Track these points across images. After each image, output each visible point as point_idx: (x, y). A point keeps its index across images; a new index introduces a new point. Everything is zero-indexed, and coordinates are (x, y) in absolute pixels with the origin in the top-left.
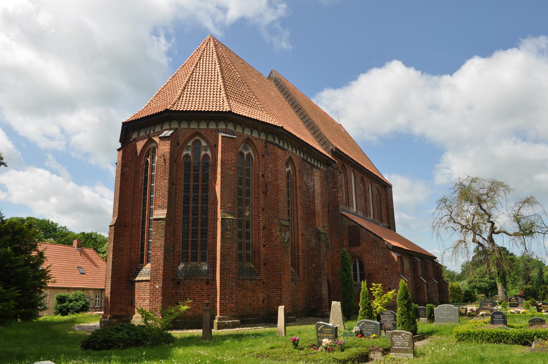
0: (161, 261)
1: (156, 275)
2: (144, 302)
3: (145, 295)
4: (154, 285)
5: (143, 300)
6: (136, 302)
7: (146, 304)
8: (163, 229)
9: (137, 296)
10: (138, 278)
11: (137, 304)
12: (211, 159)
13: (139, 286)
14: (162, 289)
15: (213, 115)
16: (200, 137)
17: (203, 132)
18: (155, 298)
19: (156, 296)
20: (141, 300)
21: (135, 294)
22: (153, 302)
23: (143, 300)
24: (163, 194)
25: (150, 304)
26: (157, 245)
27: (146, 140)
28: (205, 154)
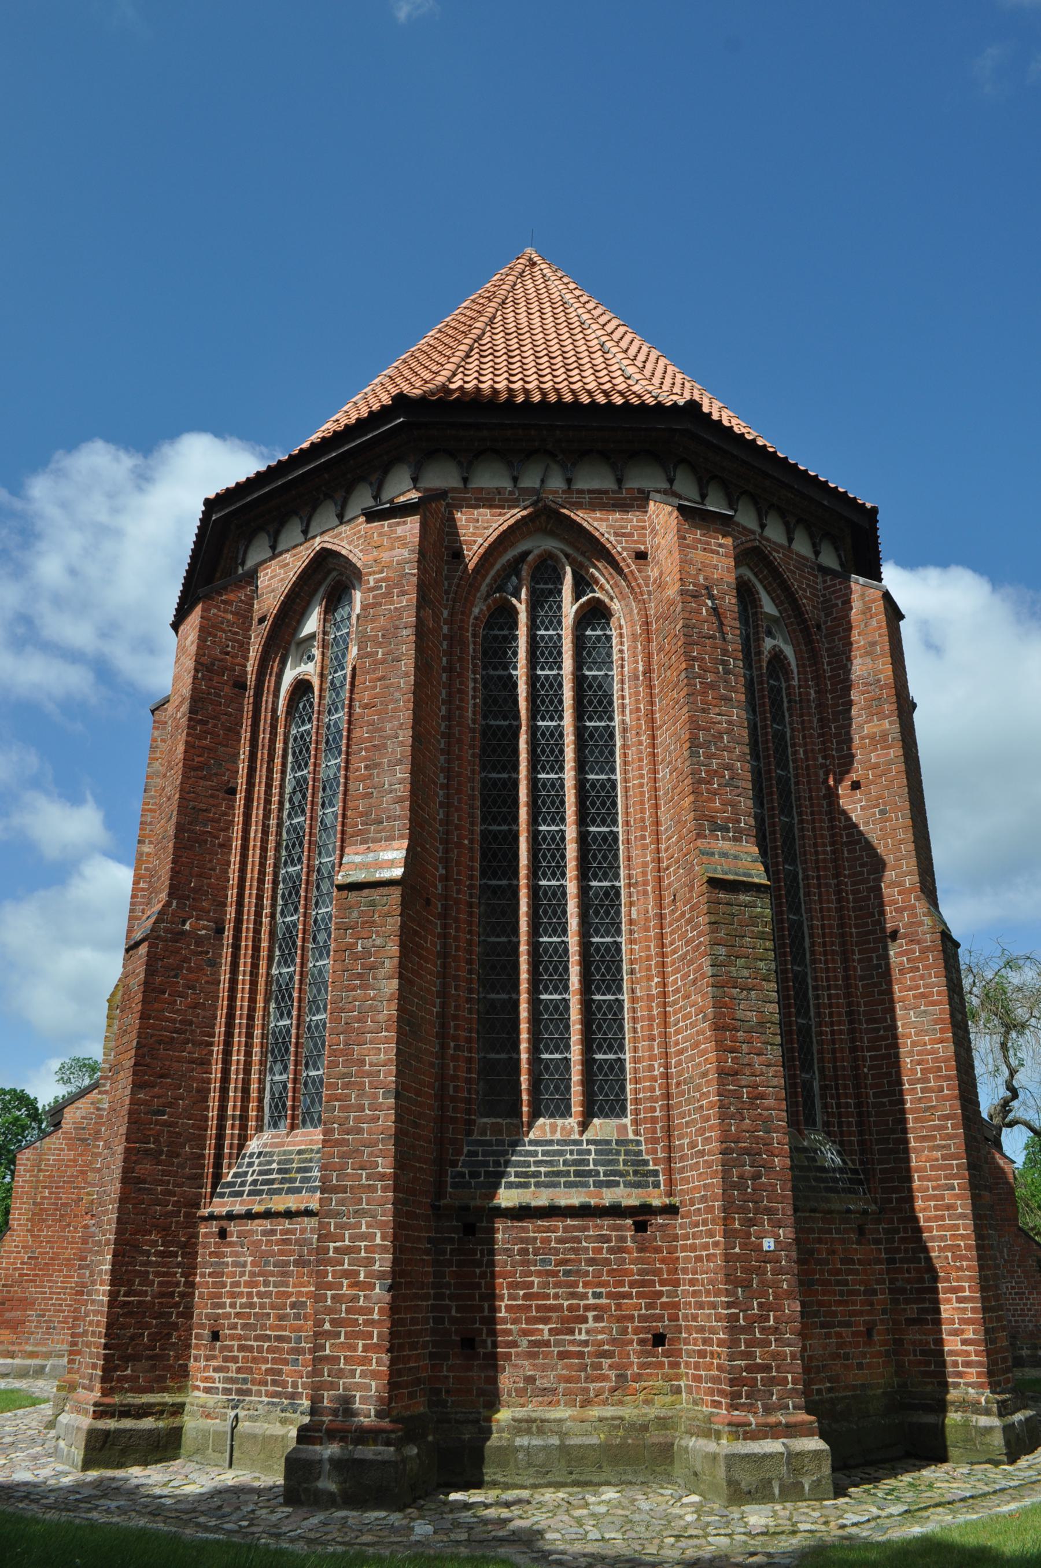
0: (770, 1102)
1: (756, 1177)
2: (572, 1332)
3: (573, 1295)
4: (748, 1235)
5: (563, 1320)
6: (509, 1332)
7: (586, 1343)
8: (761, 936)
9: (512, 1297)
10: (506, 1198)
11: (514, 1344)
12: (796, 676)
13: (522, 1240)
14: (794, 1255)
15: (826, 503)
16: (756, 575)
17: (775, 554)
18: (760, 1305)
19: (766, 1295)
20: (545, 1321)
21: (492, 1286)
22: (748, 1329)
23: (563, 1320)
24: (729, 767)
25: (733, 1343)
26: (739, 1015)
27: (515, 514)
28: (775, 646)
